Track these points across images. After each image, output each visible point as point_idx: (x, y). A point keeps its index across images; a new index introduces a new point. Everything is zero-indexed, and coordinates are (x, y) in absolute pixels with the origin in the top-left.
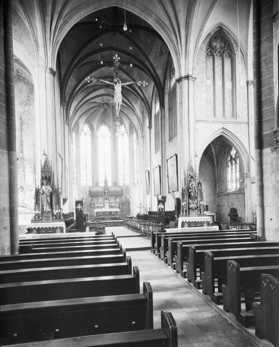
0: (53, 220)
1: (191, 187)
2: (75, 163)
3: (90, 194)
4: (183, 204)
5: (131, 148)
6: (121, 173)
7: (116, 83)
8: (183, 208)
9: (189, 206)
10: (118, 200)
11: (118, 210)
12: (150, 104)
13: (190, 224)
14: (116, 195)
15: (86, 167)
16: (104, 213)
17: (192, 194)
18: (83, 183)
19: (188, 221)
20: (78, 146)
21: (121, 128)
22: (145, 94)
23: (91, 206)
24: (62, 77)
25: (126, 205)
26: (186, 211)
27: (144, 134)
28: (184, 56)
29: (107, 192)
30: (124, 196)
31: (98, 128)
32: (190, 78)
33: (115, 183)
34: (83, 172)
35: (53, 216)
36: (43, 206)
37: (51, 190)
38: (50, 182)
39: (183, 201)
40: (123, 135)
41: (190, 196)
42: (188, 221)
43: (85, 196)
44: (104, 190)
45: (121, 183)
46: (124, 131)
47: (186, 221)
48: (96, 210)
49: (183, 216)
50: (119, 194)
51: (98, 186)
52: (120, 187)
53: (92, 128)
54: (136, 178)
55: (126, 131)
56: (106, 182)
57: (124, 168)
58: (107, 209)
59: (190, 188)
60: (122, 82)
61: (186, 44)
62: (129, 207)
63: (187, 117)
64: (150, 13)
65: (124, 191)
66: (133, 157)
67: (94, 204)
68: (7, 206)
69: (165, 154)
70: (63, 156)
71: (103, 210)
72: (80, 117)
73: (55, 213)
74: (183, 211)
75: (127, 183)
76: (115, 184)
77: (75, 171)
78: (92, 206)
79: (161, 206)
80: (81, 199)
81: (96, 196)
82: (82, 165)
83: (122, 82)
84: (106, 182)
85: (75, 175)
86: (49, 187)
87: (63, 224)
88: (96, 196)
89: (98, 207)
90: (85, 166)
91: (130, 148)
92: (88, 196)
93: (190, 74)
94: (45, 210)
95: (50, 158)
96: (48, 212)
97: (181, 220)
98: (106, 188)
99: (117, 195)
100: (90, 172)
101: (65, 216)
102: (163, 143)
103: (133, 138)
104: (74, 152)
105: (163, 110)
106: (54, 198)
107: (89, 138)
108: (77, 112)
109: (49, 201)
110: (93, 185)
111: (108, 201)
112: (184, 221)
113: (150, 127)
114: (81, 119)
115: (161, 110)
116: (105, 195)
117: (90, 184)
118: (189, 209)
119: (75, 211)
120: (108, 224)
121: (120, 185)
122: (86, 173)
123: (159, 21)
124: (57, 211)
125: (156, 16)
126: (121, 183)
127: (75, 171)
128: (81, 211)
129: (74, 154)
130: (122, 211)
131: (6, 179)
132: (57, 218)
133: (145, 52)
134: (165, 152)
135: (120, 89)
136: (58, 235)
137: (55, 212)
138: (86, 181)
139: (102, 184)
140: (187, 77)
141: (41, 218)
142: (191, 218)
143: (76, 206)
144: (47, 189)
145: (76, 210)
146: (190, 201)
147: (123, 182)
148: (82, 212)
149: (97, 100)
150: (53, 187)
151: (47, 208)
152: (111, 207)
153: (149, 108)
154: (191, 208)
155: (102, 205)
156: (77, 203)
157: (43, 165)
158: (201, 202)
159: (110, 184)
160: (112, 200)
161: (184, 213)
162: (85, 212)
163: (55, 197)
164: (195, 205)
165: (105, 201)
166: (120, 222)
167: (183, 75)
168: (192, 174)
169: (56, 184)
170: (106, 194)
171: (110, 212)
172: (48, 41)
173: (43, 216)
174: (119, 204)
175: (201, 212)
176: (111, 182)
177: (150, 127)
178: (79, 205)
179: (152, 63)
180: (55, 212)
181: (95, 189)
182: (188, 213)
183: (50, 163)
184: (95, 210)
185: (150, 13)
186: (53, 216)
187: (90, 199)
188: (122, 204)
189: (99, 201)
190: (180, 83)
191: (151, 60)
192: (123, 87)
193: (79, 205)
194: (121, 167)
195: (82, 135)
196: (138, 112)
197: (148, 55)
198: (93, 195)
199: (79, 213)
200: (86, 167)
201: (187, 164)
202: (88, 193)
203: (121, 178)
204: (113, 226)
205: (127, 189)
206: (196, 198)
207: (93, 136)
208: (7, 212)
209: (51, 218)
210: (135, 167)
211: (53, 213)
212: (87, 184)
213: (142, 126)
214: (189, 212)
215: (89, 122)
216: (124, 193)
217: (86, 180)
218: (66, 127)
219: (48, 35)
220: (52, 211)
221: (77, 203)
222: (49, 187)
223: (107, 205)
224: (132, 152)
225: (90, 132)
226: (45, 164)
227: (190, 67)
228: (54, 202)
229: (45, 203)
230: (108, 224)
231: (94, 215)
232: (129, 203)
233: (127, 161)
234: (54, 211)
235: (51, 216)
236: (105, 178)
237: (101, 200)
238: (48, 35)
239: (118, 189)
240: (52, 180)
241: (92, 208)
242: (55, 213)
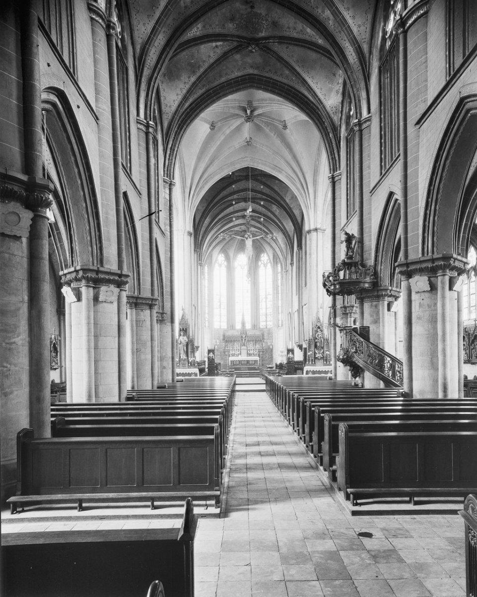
0: (189, 367)
1: (317, 337)
2: (207, 301)
3: (224, 339)
4: (309, 354)
5: (275, 281)
6: (262, 311)
7: (247, 239)
8: (309, 357)
9: (315, 356)
10: (257, 346)
11: (257, 358)
12: (292, 238)
13: (314, 372)
14: (256, 341)
15: (220, 305)
16: (240, 362)
17: (318, 344)
18: (216, 325)
19: (312, 370)
20: (211, 281)
21: (263, 256)
22: (287, 227)
23: (225, 353)
24: (197, 223)
25: (267, 353)
26: (312, 360)
27: (287, 269)
28: (313, 210)
29: (244, 336)
30: (265, 341)
31: (235, 256)
32: (318, 230)
33: (254, 325)
34: (216, 311)
35: (189, 363)
36: (180, 354)
37: (187, 340)
38: (186, 333)
39: (309, 351)
40: (265, 266)
41: (316, 346)
42: (312, 370)
43: (218, 341)
44: (241, 333)
45: (262, 325)
46: (267, 260)
47: (310, 371)
48: (231, 358)
49: (309, 365)
50: (260, 339)
51: (235, 329)
52: (261, 330)
53: (228, 258)
54: (280, 319)
55: (268, 261)
56: (243, 324)
57: (266, 306)
58: (244, 357)
59: (316, 339)
60: (253, 237)
61: (315, 198)
62: (272, 355)
63: (315, 268)
64: (281, 170)
65: (266, 335)
66: (278, 293)
67: (229, 351)
68: (171, 356)
69: (302, 299)
70: (196, 305)
71: (240, 358)
72: (217, 245)
73: (190, 361)
74: (309, 360)
75: (270, 324)
76: (255, 326)
77: (207, 312)
78: (227, 353)
79: (291, 355)
80: (213, 348)
81: (231, 341)
82: (216, 303)
83: (253, 237)
84: (243, 324)
85: (207, 315)
86: (185, 338)
87: (197, 371)
88: (231, 341)
89: (233, 355)
90: (219, 304)
91: (273, 281)
92: (222, 341)
93: (318, 227)
94: (181, 358)
95: (186, 311)
96: (185, 360)
97: (306, 368)
98: (244, 331)
99: (258, 340)
100: (224, 312)
101: (199, 364)
102: (300, 287)
103: (277, 269)
104: (206, 289)
105: (300, 252)
106: (190, 347)
107: (224, 270)
108: (210, 246)
109: (185, 350)
110: (228, 327)
111: (245, 347)
112: (309, 370)
113: (292, 264)
114: (214, 251)
115: (299, 251)
116: (242, 340)
117: (224, 326)
118: (315, 358)
119: (206, 360)
120: (244, 375)
121: (261, 327)
122: (220, 313)
123: (288, 176)
124: (192, 359)
125: (286, 172)
126: (262, 325)
127: (207, 312)
128: (213, 359)
129: (206, 292)
130: (262, 360)
131: (170, 340)
132: (192, 364)
133: (281, 193)
134: (302, 296)
135: (251, 243)
136: (193, 377)
137: (191, 360)
138: (220, 323)
139: (238, 326)
140: (316, 230)
141: (178, 365)
142: (317, 367)
143: (208, 354)
144: (184, 339)
145: (209, 358)
146: (316, 351)
147: (265, 323)
148: (214, 360)
149: (236, 229)
150: (188, 338)
151: (183, 356)
152: (249, 355)
153: (291, 242)
154: (317, 358)
155: (238, 353)
156: (209, 351)
157: (180, 318)
158: (327, 352)
159: (248, 326)
160: (251, 346)
161: (310, 363)
162: (217, 361)
163: (190, 347)
164: (321, 355)
165: (242, 348)
166: (257, 373)
167: (312, 227)
168: (319, 325)
169: (191, 335)
170: (244, 338)
171: (248, 362)
172: (186, 207)
173: (180, 363)
174: (259, 352)
175: (327, 362)
176: (250, 323)
177: (292, 264)
178: (211, 353)
179: (289, 203)
180: (191, 360)
181: (230, 333)
182: (313, 362)
183: (187, 316)
184: (230, 358)
185: (281, 170)
186: (189, 363)
187: (224, 345)
188: (263, 352)
189: (235, 347)
190: (310, 234)
191: (287, 201)
192: (253, 241)
193: (211, 353)
194: (262, 305)
195: (217, 266)
196: (280, 243)
197: (283, 196)
198: (228, 340)
199: (211, 361)
200: (220, 305)
201: (315, 315)
202: (222, 338)
203: (262, 318)
204: (249, 377)
205: (270, 333)
206: (323, 348)
207: (230, 269)
208: (171, 359)
209: (187, 365)
210: (280, 305)
211: (188, 361)
212: (220, 326)
213: (286, 259)
214: (315, 362)
215: (224, 251)
216: (265, 338)
217: (220, 322)
218: (199, 267)
219: (186, 204)
220: (188, 359)
221: (209, 351)
222: (185, 338)
223: (244, 352)
224: (275, 288)
225: (226, 263)
226: (182, 317)
227: (319, 220)
228: (189, 350)
229: (182, 352)
230: (244, 375)
231: (229, 364)
232: (272, 350)
233: (270, 297)
234: (190, 358)
235: (187, 363)
236: (243, 318)
237: (237, 346)
238: (186, 204)
239: (258, 333)
240: (188, 331)
241: (227, 355)
242: (190, 361)
